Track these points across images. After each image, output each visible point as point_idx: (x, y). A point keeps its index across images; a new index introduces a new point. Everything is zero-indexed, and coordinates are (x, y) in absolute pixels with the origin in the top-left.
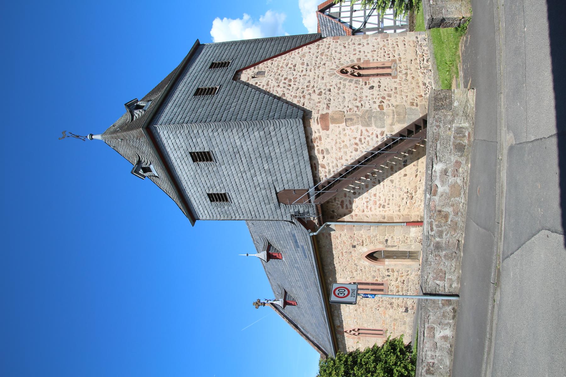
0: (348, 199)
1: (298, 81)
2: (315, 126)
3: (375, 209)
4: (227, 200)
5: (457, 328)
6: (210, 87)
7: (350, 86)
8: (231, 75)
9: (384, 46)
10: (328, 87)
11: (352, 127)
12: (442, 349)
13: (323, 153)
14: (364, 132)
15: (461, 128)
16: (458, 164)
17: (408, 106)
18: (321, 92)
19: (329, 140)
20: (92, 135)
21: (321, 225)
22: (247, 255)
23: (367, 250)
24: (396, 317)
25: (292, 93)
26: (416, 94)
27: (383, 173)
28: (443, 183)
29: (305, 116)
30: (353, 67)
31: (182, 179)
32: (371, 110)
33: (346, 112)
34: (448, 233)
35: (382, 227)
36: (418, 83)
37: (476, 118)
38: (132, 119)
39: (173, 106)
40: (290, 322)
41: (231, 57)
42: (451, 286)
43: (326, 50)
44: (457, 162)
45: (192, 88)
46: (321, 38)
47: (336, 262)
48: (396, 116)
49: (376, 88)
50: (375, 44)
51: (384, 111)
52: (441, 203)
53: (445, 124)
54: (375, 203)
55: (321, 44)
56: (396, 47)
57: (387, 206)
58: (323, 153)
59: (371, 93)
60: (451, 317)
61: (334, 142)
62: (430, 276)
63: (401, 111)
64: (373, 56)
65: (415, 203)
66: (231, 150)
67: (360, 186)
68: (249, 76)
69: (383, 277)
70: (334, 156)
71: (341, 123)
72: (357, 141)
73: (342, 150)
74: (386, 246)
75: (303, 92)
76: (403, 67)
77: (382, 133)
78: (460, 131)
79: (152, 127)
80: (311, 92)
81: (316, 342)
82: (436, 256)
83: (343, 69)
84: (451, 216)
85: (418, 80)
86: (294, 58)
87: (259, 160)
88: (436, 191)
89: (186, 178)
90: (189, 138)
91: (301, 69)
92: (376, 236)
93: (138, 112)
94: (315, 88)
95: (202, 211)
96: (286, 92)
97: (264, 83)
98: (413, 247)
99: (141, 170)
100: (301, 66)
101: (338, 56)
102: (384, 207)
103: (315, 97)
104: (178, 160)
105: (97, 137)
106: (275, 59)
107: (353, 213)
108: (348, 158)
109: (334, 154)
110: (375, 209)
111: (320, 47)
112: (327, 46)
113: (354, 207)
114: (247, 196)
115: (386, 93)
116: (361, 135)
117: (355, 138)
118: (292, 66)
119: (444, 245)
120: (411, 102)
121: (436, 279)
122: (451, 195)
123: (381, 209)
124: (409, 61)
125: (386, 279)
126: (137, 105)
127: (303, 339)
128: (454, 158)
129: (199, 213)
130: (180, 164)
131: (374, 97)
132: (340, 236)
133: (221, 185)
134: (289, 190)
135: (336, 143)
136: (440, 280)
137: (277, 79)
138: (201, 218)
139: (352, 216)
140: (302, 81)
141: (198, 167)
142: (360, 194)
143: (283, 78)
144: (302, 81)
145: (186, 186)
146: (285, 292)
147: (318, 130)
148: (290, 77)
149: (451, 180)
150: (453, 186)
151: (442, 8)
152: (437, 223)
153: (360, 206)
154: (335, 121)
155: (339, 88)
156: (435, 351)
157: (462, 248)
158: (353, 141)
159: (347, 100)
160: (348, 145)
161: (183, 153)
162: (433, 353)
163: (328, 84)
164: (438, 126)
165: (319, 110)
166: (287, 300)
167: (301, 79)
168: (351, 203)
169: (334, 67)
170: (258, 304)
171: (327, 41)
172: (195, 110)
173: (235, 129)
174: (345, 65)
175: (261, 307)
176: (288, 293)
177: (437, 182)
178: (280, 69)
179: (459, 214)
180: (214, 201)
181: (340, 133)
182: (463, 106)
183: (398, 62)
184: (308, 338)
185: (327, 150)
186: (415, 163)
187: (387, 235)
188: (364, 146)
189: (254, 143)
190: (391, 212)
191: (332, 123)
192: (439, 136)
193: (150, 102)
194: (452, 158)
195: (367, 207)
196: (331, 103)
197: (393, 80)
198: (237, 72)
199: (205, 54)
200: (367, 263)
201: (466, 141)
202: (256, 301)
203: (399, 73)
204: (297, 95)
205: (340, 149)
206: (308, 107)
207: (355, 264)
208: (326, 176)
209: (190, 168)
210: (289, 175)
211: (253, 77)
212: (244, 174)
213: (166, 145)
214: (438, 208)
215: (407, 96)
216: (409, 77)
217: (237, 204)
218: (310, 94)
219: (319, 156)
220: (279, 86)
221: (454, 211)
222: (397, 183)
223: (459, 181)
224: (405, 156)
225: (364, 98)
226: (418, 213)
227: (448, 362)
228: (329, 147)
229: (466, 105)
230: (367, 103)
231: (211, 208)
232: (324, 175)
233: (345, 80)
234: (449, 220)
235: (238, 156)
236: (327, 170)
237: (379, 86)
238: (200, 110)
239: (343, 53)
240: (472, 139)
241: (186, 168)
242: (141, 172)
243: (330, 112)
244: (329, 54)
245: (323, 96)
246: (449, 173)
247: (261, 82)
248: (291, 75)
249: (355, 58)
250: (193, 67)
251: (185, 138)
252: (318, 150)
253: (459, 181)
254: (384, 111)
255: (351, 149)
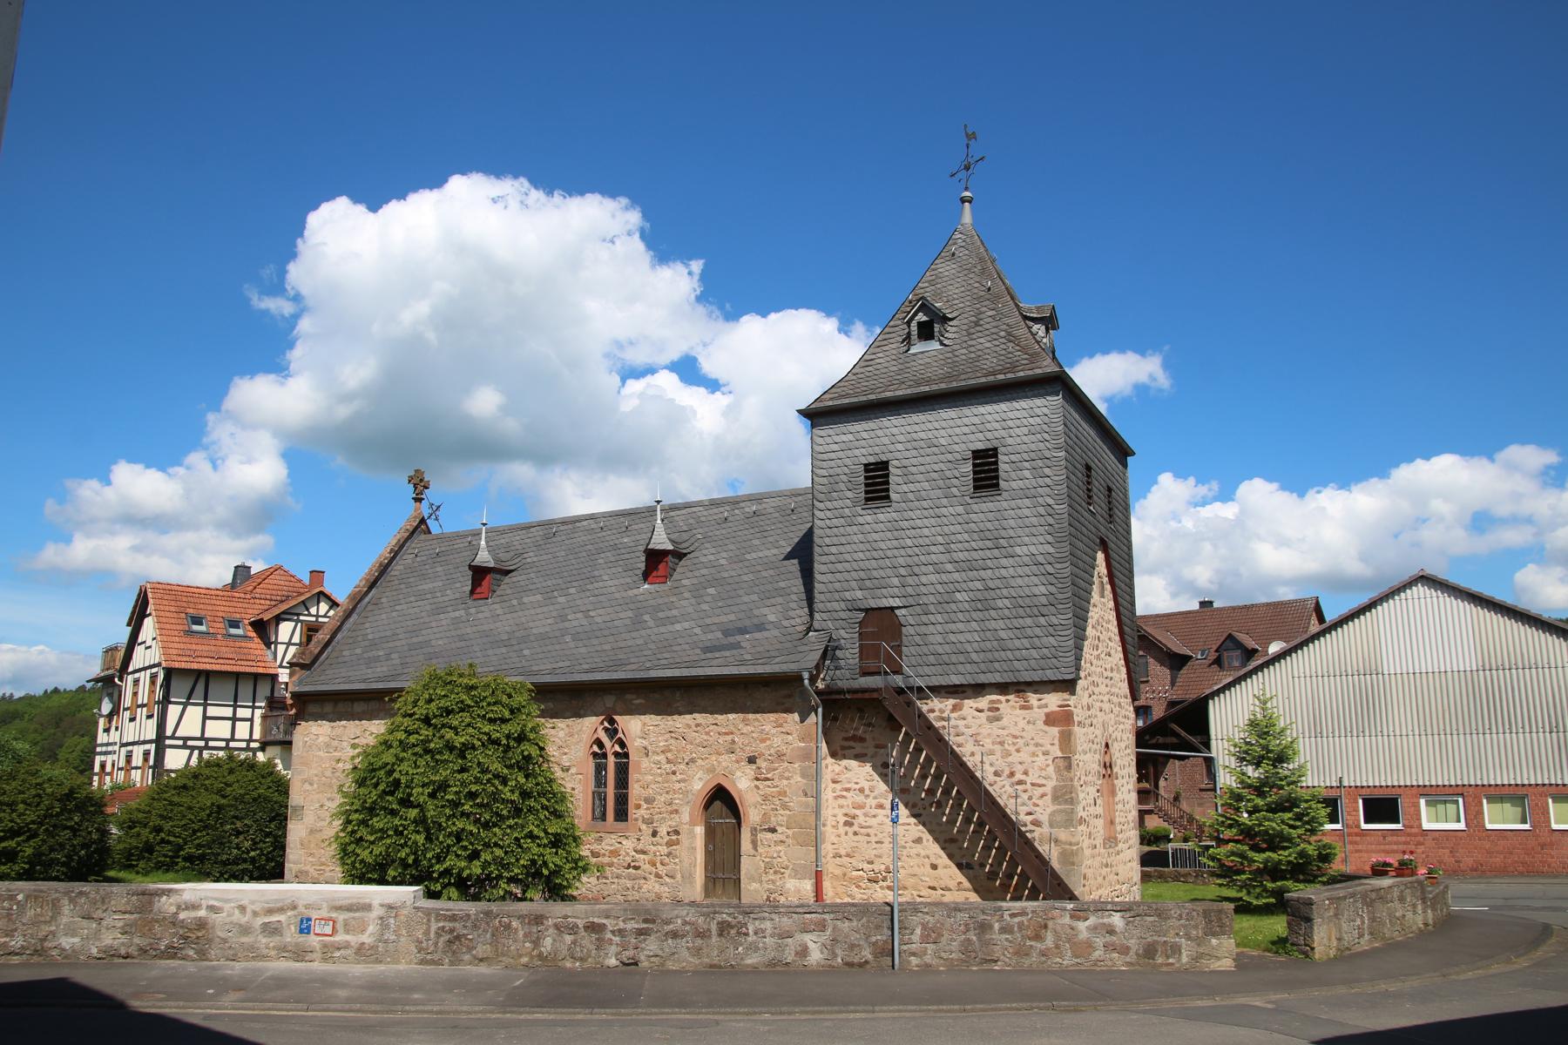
0: (871, 751)
2: (1053, 700)
3: (841, 807)
4: (867, 499)
5: (827, 970)
11: (1051, 769)
12: (780, 948)
13: (990, 710)
14: (1041, 790)
16: (1125, 950)
19: (1022, 724)
23: (742, 784)
27: (940, 824)
28: (1094, 929)
37: (1351, 956)
40: (384, 569)
42: (914, 954)
44: (1128, 948)
47: (700, 718)
52: (1058, 928)
53: (1184, 926)
57: (850, 830)
58: (990, 710)
60: (848, 959)
62: (928, 918)
65: (858, 887)
67: (908, 776)
69: (649, 822)
70: (984, 731)
71: (1061, 750)
72: (1019, 776)
73: (998, 747)
74: (754, 831)
77: (1036, 823)
78: (1176, 949)
81: (339, 636)
88: (1079, 919)
90: (1033, 455)
92: (785, 807)
95: (837, 439)
98: (755, 885)
99: (925, 318)
102: (846, 824)
104: (976, 420)
105: (967, 218)
107: (830, 760)
109: (989, 731)
110: (841, 807)
113: (845, 762)
117: (1026, 773)
121: (924, 926)
123: (842, 819)
125: (644, 827)
128: (1132, 943)
129: (831, 432)
130: (966, 421)
132: (786, 733)
133: (911, 496)
135: (1015, 737)
136: (922, 935)
142: (883, 776)
145: (909, 420)
147: (1046, 706)
149: (1099, 942)
150: (1089, 945)
153: (849, 775)
156: (772, 936)
157: (985, 967)
158: (1019, 769)
160: (1010, 759)
161: (997, 434)
162: (769, 932)
166: (492, 575)
168: (859, 757)
170: (419, 485)
173: (1052, 550)
176: (507, 579)
177: (1092, 920)
180: (866, 471)
181: (1037, 745)
185: (998, 719)
186: (967, 884)
187: (790, 832)
188: (1008, 788)
189: (1019, 581)
195: (847, 790)
200: (700, 785)
201: (1160, 961)
205: (1002, 743)
207: (693, 761)
208: (933, 711)
209: (956, 439)
210: (939, 639)
212: (941, 548)
213: (1015, 404)
214: (1050, 924)
219: (984, 702)
222: (914, 851)
223: (1097, 954)
224: (983, 866)
227: (750, 960)
228: (1005, 722)
232: (936, 709)
235: (989, 544)
240: (1164, 969)
241: (957, 430)
242: (922, 317)
246: (1109, 938)
251: (1033, 447)
252: (999, 701)
253: (1097, 953)
255: (1000, 764)
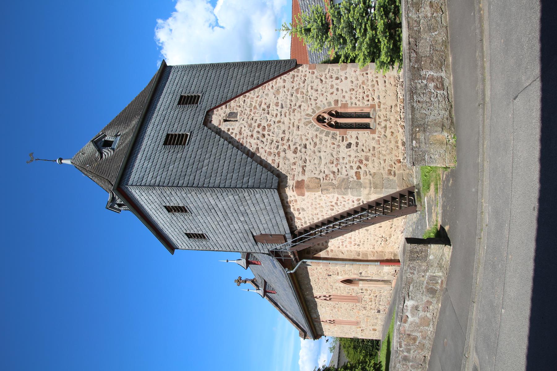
1: (272, 130)
2: (290, 193)
6: (180, 133)
7: (328, 142)
8: (201, 118)
9: (363, 83)
10: (304, 142)
11: (328, 195)
15: (434, 276)
17: (385, 173)
18: (296, 148)
20: (61, 159)
21: (297, 262)
22: (227, 261)
24: (369, 315)
25: (266, 148)
26: (394, 158)
28: (413, 315)
29: (279, 182)
30: (330, 114)
31: (159, 222)
32: (348, 179)
33: (322, 179)
34: (415, 351)
35: (356, 265)
36: (397, 142)
37: (450, 271)
38: (102, 157)
39: (143, 159)
41: (200, 89)
43: (302, 85)
44: (428, 301)
45: (161, 133)
46: (297, 66)
48: (372, 188)
49: (353, 147)
50: (354, 80)
51: (361, 181)
53: (419, 272)
54: (351, 243)
55: (296, 74)
56: (376, 85)
59: (348, 154)
61: (310, 204)
63: (379, 182)
64: (351, 98)
66: (206, 207)
68: (220, 118)
70: (310, 213)
75: (278, 147)
76: (382, 117)
78: (433, 278)
79: (123, 188)
80: (286, 147)
81: (295, 320)
82: (403, 365)
83: (320, 115)
84: (419, 339)
85: (397, 136)
86: (267, 95)
87: (235, 215)
89: (163, 222)
91: (275, 112)
93: (107, 151)
94: (290, 143)
96: (260, 145)
97: (236, 131)
100: (275, 108)
101: (315, 94)
102: (359, 245)
103: (290, 155)
106: (247, 94)
107: (329, 249)
108: (324, 214)
111: (295, 79)
112: (303, 78)
114: (225, 237)
115: (364, 154)
116: (337, 200)
118: (265, 107)
119: (411, 358)
120: (389, 170)
122: (421, 324)
123: (356, 246)
124: (389, 108)
126: (106, 141)
127: (282, 316)
128: (425, 299)
131: (351, 159)
134: (266, 235)
137: (250, 126)
138: (180, 247)
139: (328, 251)
140: (276, 130)
141: (173, 216)
143: (256, 125)
144: (276, 130)
146: (265, 281)
148: (264, 123)
149: (421, 314)
151: (424, 152)
152: (406, 343)
154: (309, 189)
155: (315, 144)
157: (427, 362)
159: (323, 162)
160: (324, 207)
163: (304, 138)
164: (413, 273)
165: (294, 175)
166: (267, 290)
167: (276, 128)
168: (327, 242)
169: (310, 111)
171: (303, 69)
172: (167, 167)
174: (322, 110)
175: (242, 284)
178: (253, 111)
179: (427, 338)
182: (439, 259)
183: (377, 108)
184: (287, 316)
190: (366, 249)
191: (308, 191)
192: (412, 280)
193: (119, 138)
194: (424, 298)
196: (307, 165)
197: (372, 136)
198: (208, 112)
199: (173, 80)
202: (237, 278)
203: (378, 126)
204: (272, 151)
206: (283, 169)
211: (225, 121)
214: (407, 332)
215: (385, 160)
216: (388, 133)
217: (215, 241)
218: (284, 151)
220: (252, 136)
221: (422, 335)
225: (341, 160)
226: (392, 250)
228: (305, 207)
229: (441, 258)
230: (343, 167)
231: (189, 242)
233: (322, 132)
234: (418, 342)
235: (213, 211)
236: (303, 221)
237: (357, 144)
238: (171, 167)
239: (319, 92)
242: (116, 206)
243: (305, 178)
244: (305, 91)
245: (299, 154)
247: (233, 129)
248: (265, 121)
249: (331, 99)
250: (161, 100)
253: (428, 315)
254: (361, 181)
